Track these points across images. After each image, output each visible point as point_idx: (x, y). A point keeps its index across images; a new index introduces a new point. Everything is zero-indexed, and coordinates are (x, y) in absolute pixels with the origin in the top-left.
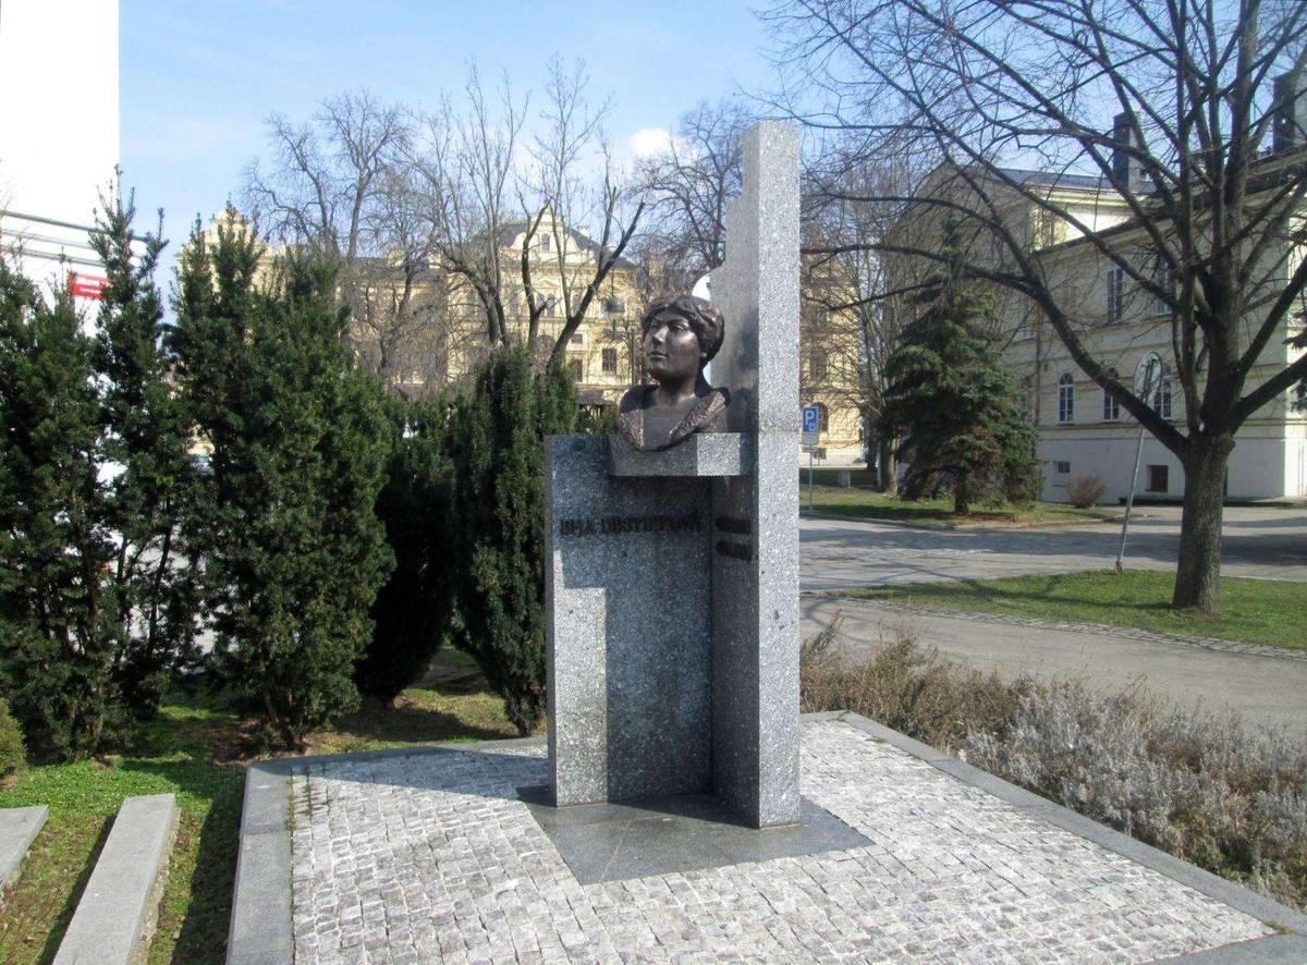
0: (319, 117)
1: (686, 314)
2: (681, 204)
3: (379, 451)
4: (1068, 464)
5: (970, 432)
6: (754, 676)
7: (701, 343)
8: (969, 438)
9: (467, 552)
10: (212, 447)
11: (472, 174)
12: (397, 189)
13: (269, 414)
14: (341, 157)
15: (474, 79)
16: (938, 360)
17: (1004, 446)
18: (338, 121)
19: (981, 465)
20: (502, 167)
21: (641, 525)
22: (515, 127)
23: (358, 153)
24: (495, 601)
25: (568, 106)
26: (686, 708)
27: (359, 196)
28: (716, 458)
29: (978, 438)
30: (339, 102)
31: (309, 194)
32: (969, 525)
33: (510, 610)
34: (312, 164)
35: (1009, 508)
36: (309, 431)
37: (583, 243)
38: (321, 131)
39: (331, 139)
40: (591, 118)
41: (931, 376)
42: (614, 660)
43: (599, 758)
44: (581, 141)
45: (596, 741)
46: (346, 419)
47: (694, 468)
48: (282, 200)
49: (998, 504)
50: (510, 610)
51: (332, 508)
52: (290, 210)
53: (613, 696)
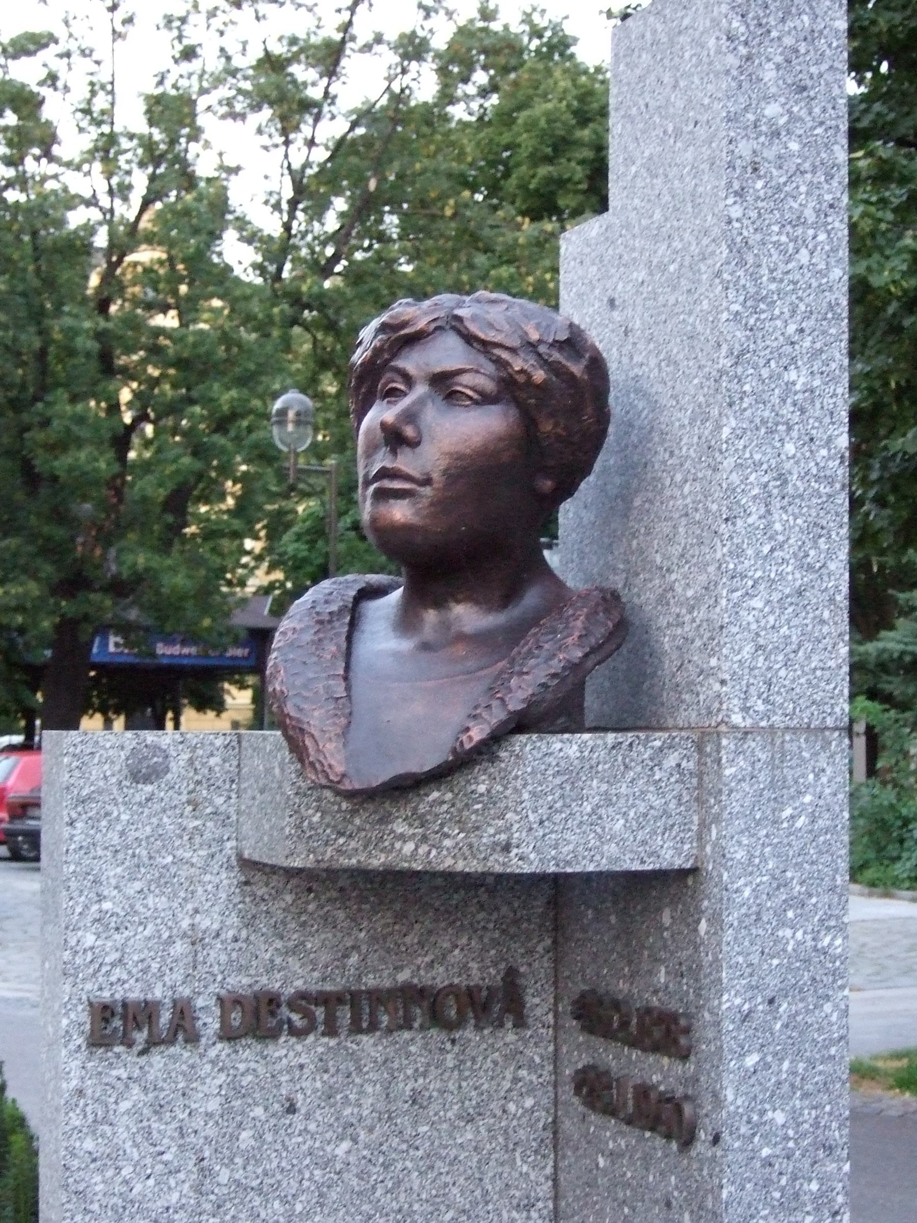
21: (345, 1015)
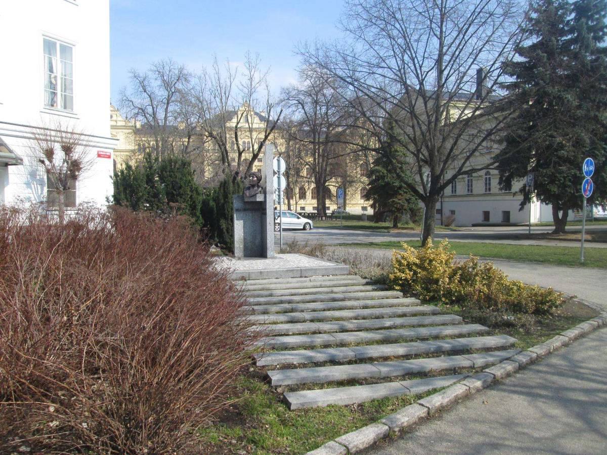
0: (151, 70)
2: (300, 106)
3: (201, 198)
5: (396, 197)
7: (258, 179)
8: (395, 200)
9: (218, 221)
10: (23, 220)
11: (215, 98)
12: (184, 99)
13: (181, 191)
14: (160, 86)
15: (216, 62)
16: (385, 172)
17: (409, 203)
18: (159, 72)
19: (400, 210)
20: (227, 94)
22: (232, 80)
23: (167, 85)
24: (225, 230)
25: (253, 71)
26: (257, 241)
27: (168, 103)
28: (260, 198)
29: (399, 200)
30: (160, 64)
31: (147, 101)
32: (396, 231)
33: (228, 232)
34: (148, 89)
35: (411, 225)
36: (188, 194)
38: (152, 75)
39: (156, 79)
40: (262, 76)
41: (383, 177)
42: (244, 233)
43: (242, 249)
44: (258, 85)
45: (242, 246)
46: (195, 192)
48: (136, 104)
49: (407, 223)
50: (228, 232)
51: (192, 210)
52: (139, 109)
53: (245, 239)
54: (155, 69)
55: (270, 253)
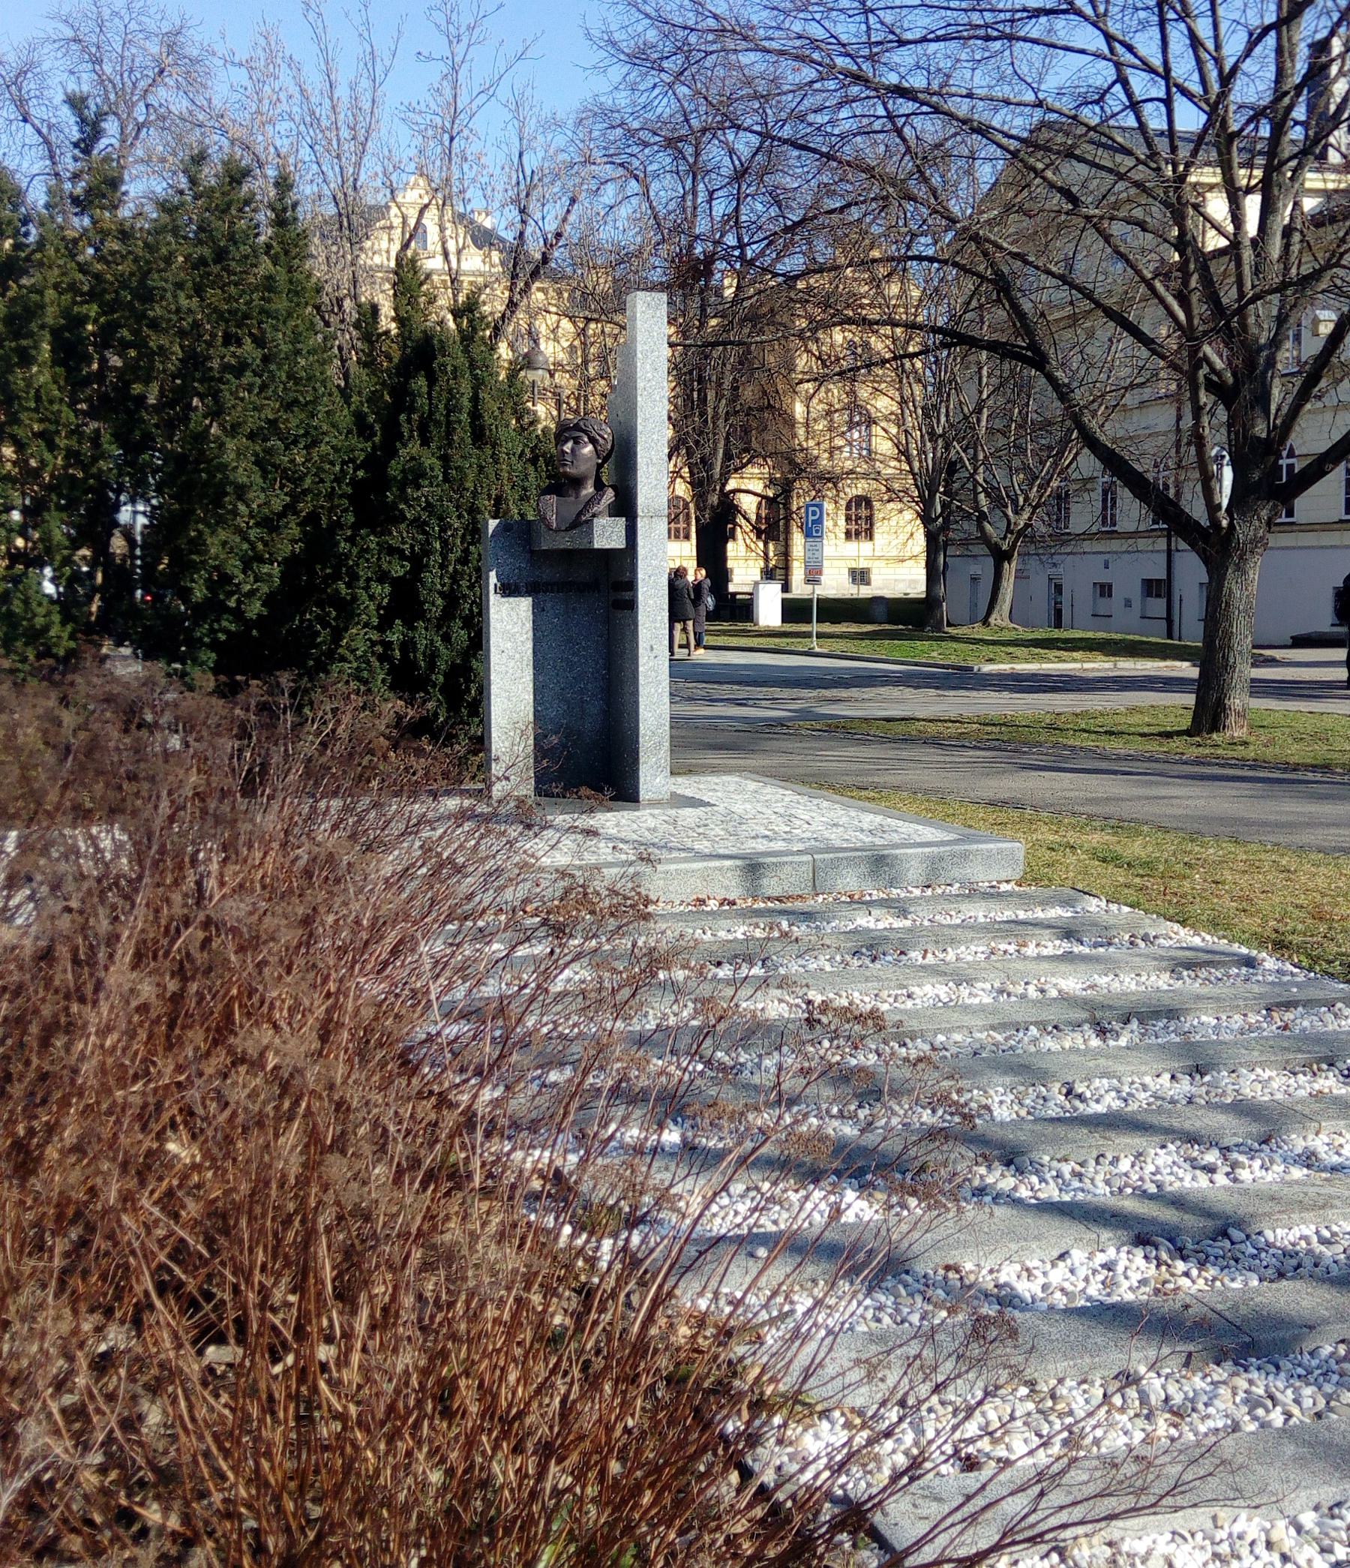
1: (585, 432)
4: (1110, 586)
6: (635, 693)
28: (607, 534)
34: (37, 112)
37: (484, 239)
42: (537, 701)
47: (591, 542)
54: (69, 33)
55: (654, 774)
